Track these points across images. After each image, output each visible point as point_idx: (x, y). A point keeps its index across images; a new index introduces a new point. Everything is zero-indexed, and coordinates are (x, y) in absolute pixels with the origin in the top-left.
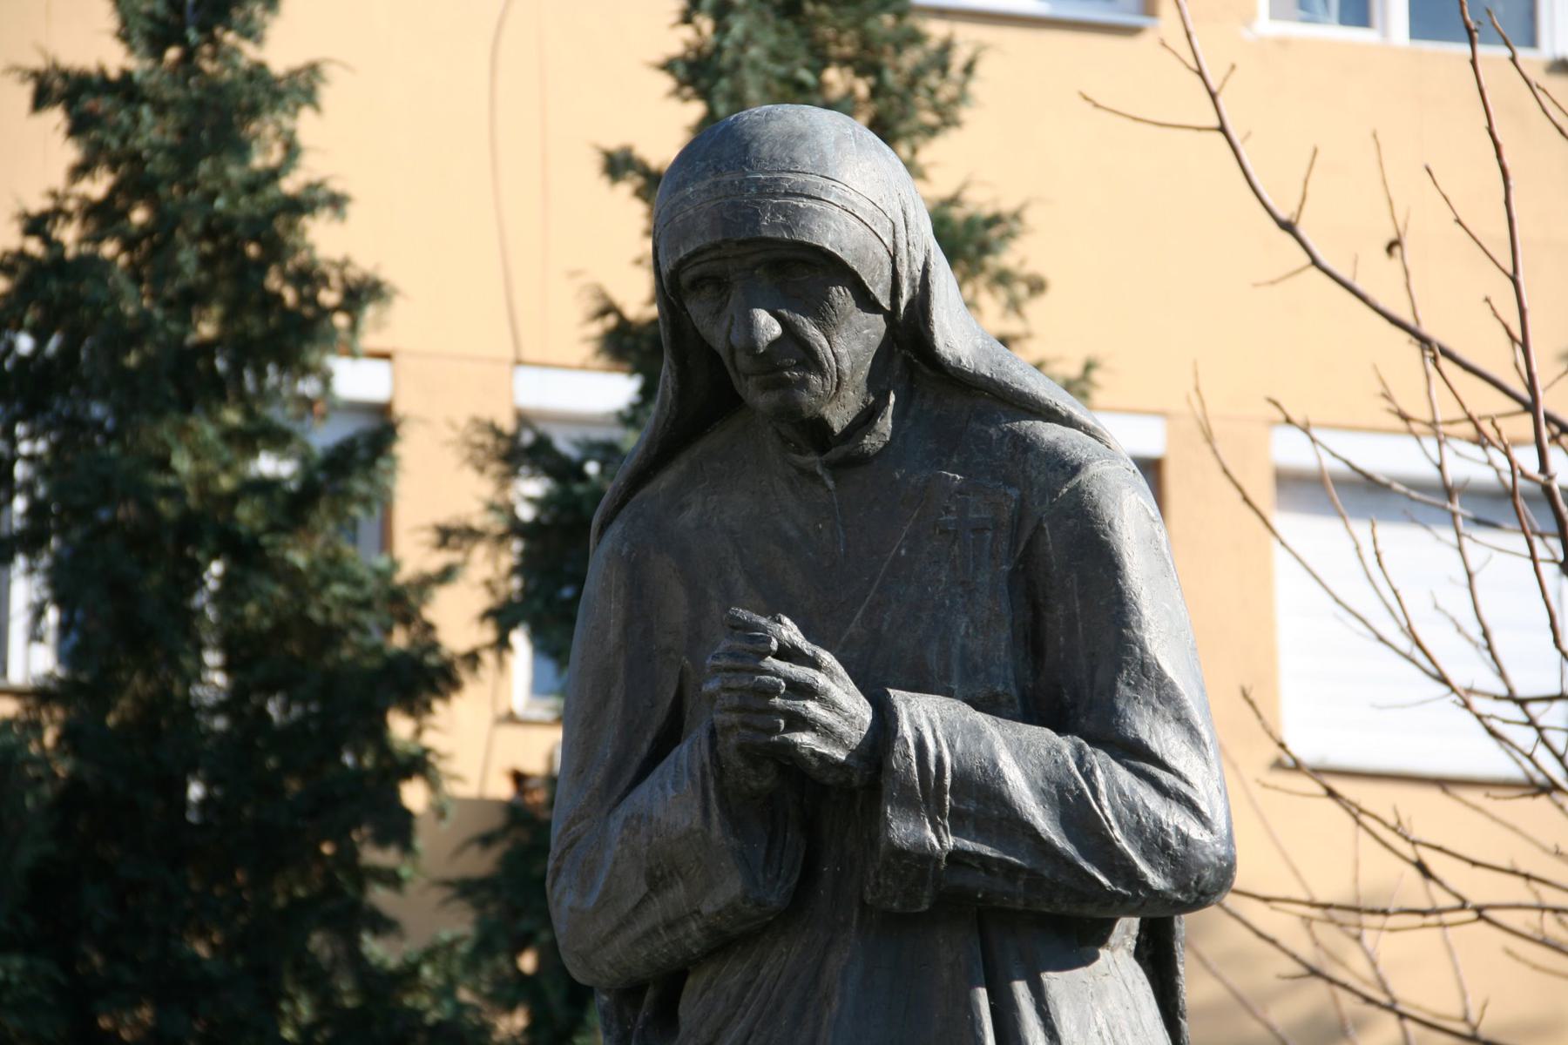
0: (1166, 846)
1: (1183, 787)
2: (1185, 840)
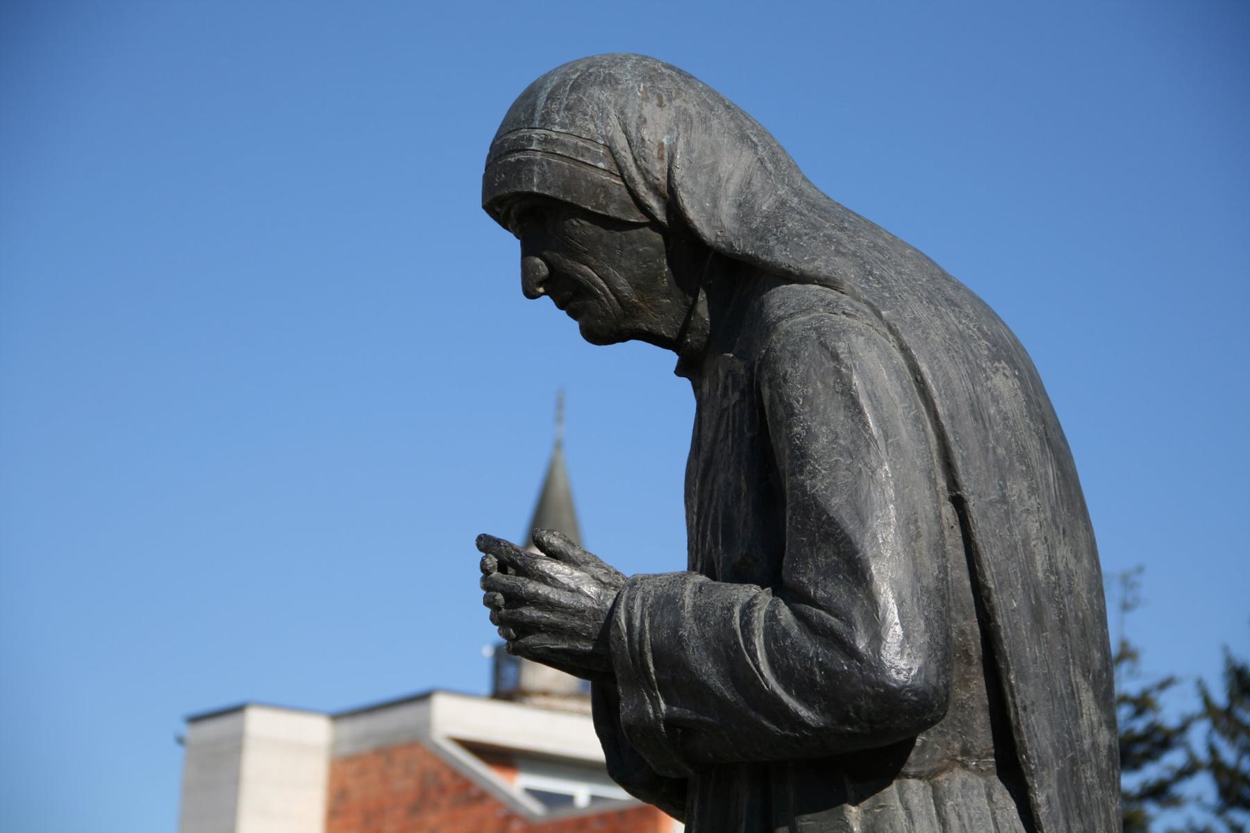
0: (813, 683)
1: (833, 621)
2: (830, 674)
